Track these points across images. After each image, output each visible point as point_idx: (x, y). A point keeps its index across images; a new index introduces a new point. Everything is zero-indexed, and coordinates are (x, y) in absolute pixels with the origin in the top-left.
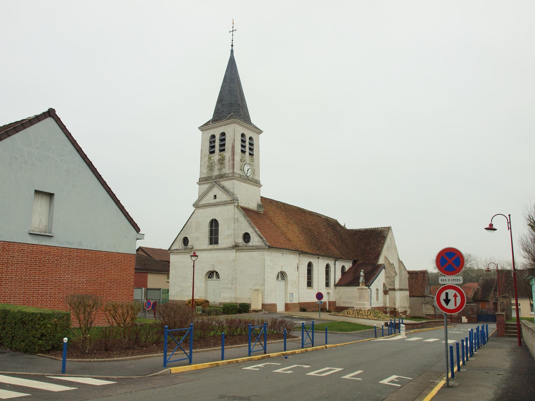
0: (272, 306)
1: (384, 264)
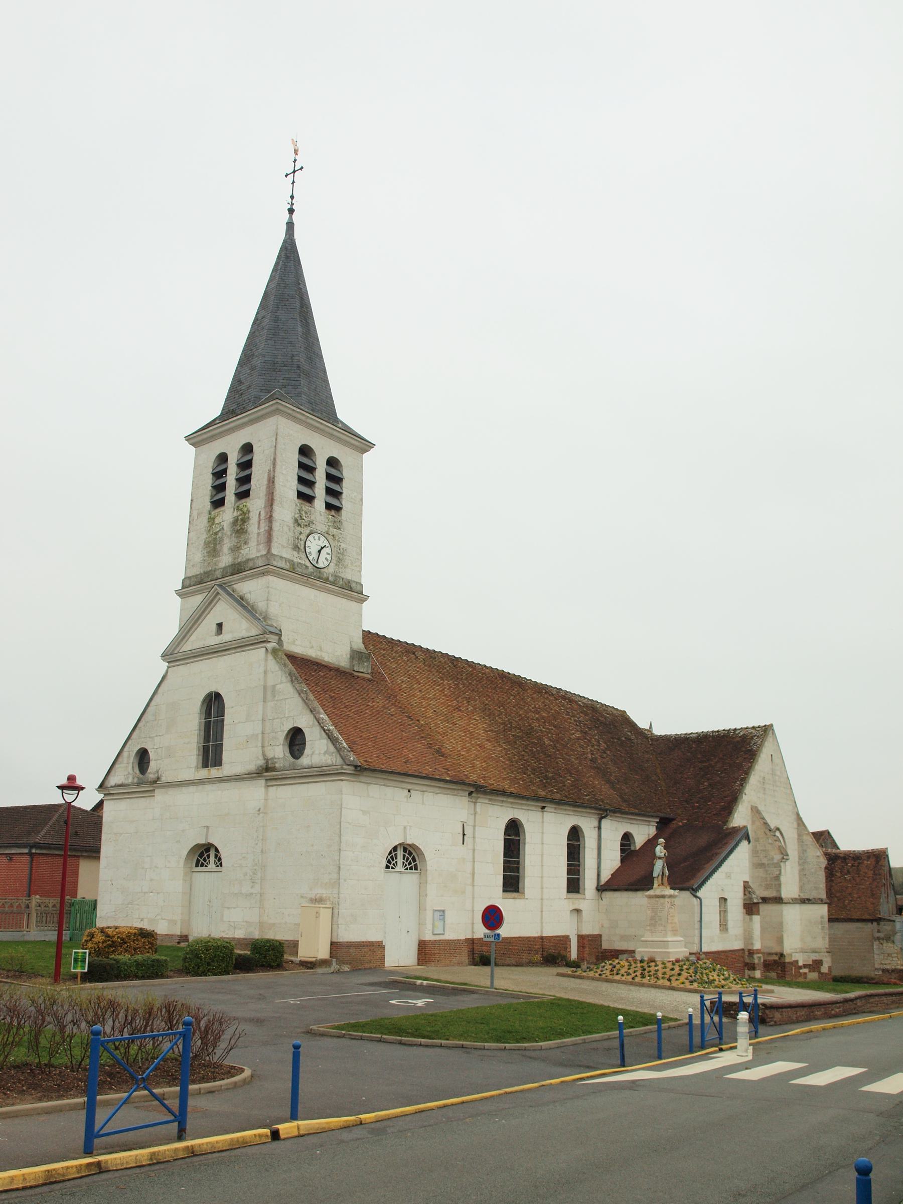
0: (366, 950)
1: (745, 827)
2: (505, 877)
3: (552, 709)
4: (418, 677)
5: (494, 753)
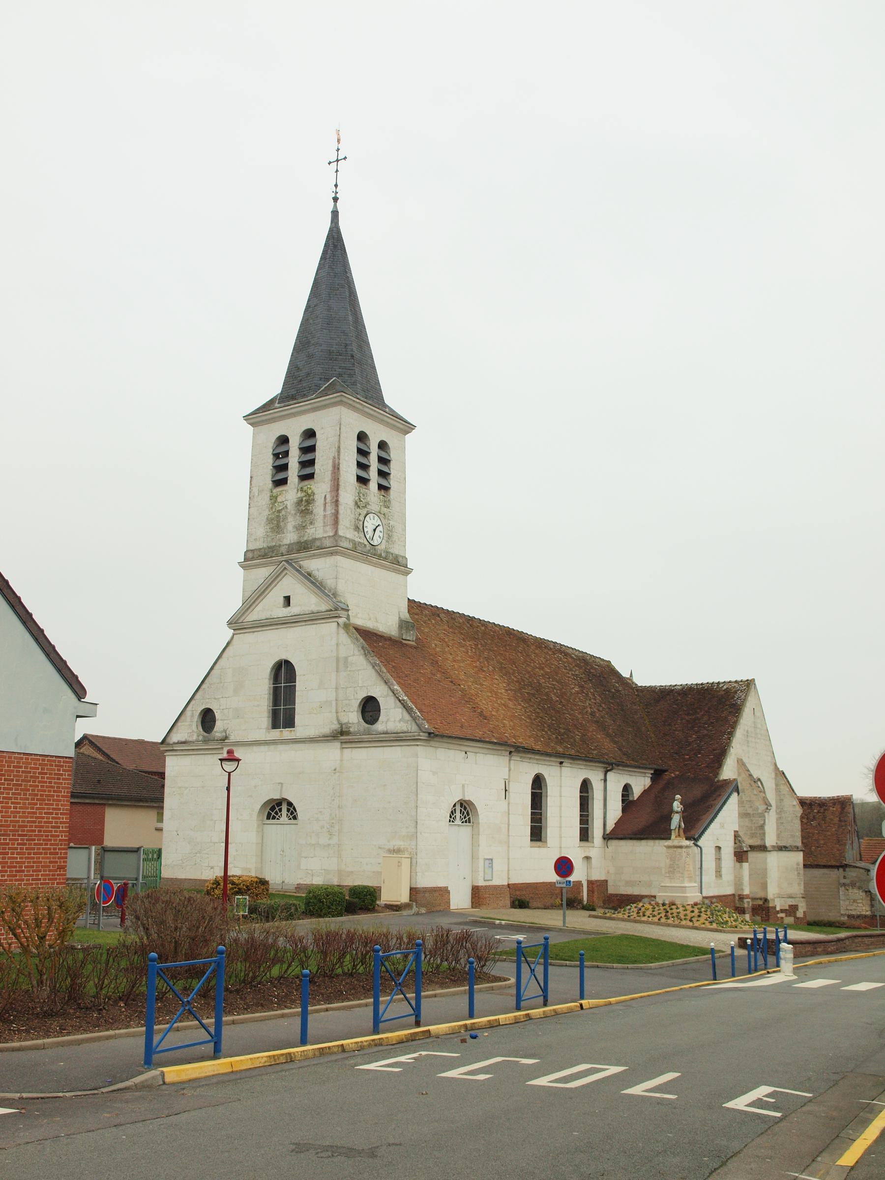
2: (532, 827)
3: (552, 664)
4: (446, 640)
5: (516, 712)
